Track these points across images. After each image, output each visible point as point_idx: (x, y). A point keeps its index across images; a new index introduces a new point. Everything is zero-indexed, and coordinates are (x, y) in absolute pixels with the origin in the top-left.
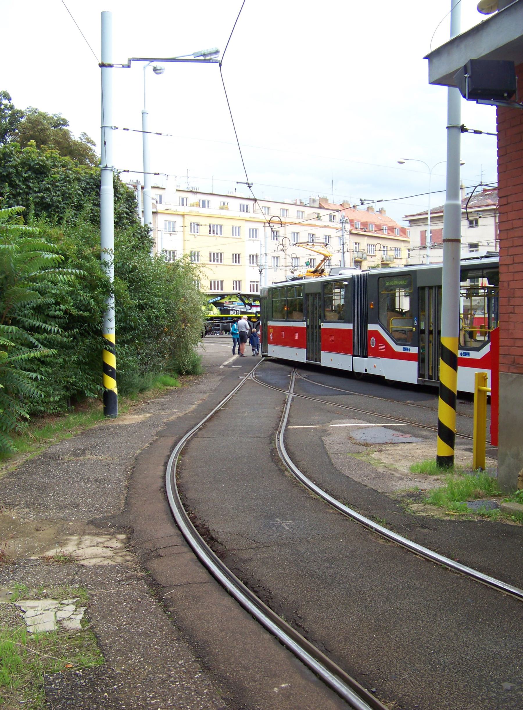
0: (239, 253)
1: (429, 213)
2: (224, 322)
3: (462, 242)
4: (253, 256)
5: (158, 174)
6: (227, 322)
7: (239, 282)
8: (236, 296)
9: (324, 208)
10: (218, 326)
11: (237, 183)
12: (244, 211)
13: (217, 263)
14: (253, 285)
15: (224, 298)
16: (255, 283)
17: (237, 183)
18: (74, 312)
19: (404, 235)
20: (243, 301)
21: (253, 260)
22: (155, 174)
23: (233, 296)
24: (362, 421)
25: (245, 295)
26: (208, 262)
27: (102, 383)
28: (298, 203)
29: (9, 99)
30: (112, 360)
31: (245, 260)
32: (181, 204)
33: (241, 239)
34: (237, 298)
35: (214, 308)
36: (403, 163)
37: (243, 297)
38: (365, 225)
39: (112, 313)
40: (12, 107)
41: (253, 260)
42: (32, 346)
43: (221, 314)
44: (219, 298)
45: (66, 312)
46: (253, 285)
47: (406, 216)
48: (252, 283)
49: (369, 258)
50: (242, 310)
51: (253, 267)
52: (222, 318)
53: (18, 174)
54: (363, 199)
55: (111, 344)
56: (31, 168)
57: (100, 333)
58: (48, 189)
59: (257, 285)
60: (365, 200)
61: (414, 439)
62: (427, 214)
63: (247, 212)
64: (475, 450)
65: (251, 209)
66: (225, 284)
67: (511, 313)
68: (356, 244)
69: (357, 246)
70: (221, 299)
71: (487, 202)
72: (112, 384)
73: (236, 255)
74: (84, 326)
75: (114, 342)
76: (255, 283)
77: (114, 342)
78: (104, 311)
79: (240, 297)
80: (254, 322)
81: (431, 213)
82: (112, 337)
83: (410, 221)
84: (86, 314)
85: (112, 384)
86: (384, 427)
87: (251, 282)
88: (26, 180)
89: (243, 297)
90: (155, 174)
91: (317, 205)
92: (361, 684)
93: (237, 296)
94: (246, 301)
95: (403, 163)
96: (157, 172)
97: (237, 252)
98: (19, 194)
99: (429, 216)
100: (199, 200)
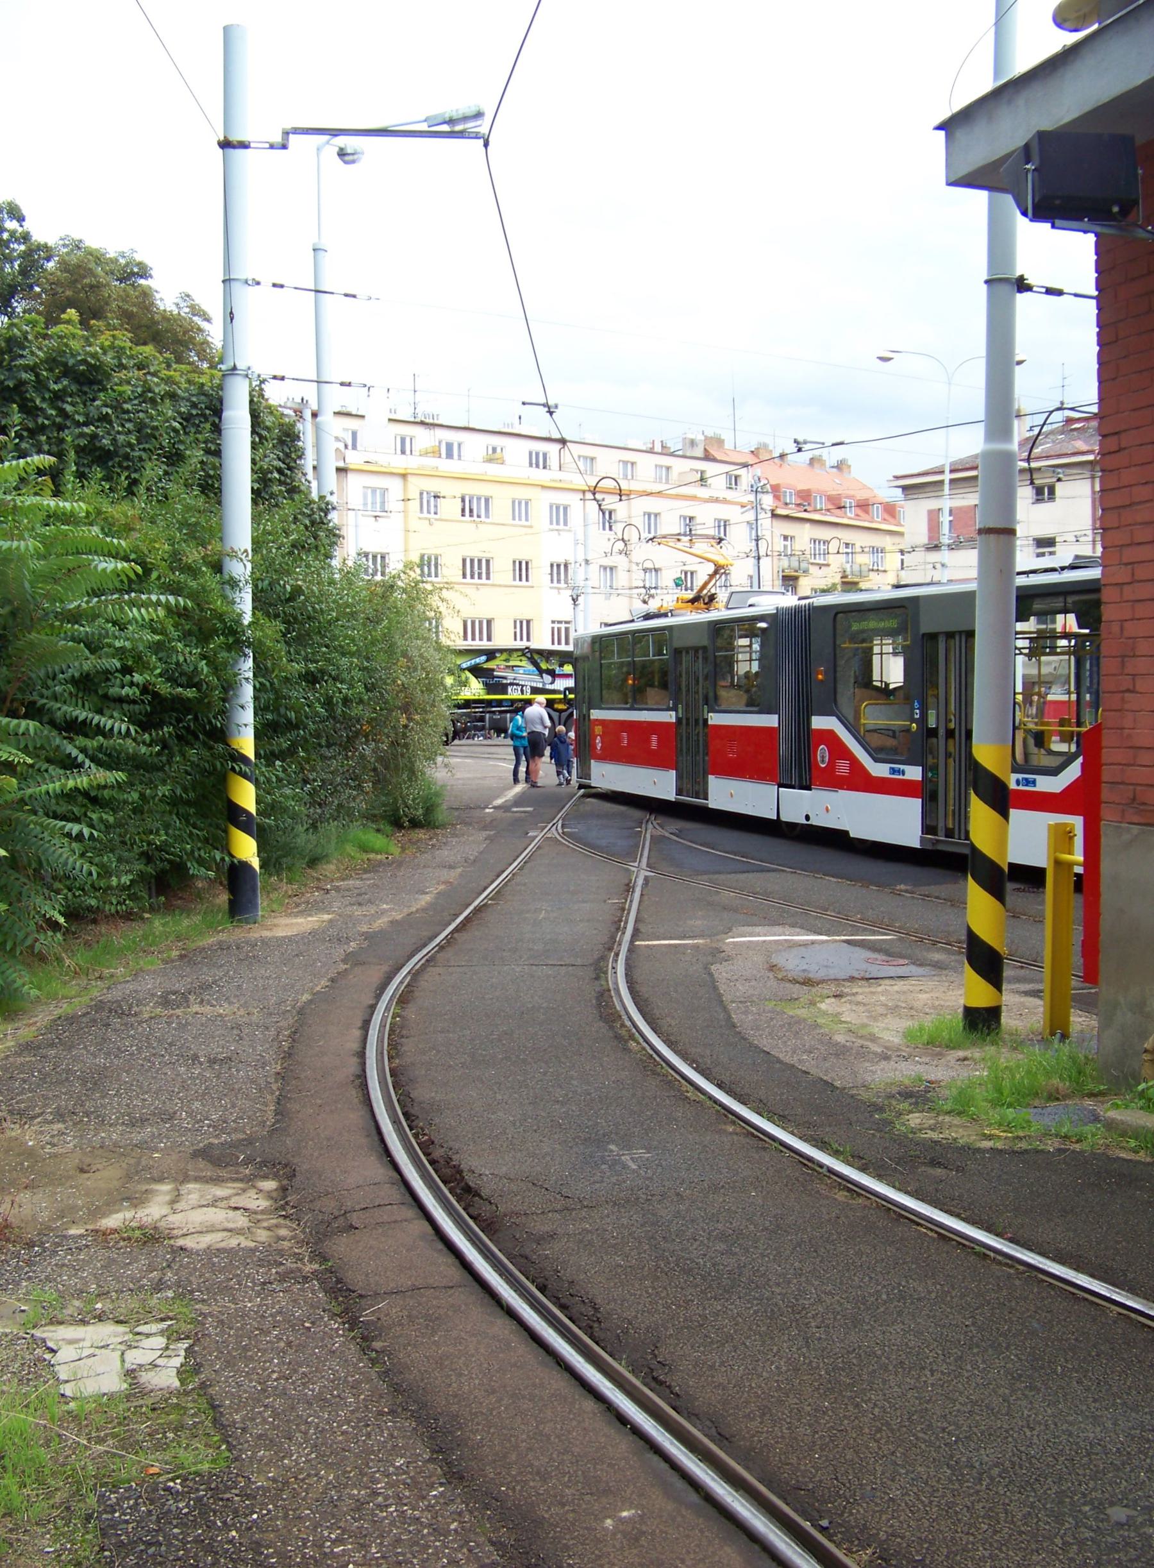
0: (527, 558)
1: (947, 470)
2: (494, 712)
3: (1019, 534)
4: (558, 566)
5: (349, 384)
6: (501, 712)
7: (528, 622)
8: (520, 653)
9: (715, 460)
10: (482, 719)
11: (524, 403)
12: (537, 466)
13: (480, 581)
14: (559, 629)
15: (494, 658)
16: (563, 626)
17: (524, 403)
18: (164, 688)
20: (535, 664)
21: (559, 573)
22: (342, 384)
23: (515, 654)
24: (798, 930)
25: (540, 652)
26: (460, 579)
27: (225, 846)
28: (658, 448)
29: (21, 219)
30: (246, 796)
31: (540, 573)
32: (399, 451)
33: (531, 527)
34: (523, 658)
35: (472, 679)
36: (889, 359)
37: (536, 657)
38: (805, 497)
39: (247, 692)
40: (26, 237)
41: (559, 573)
42: (70, 765)
43: (488, 694)
44: (484, 658)
45: (145, 689)
46: (559, 629)
47: (897, 478)
48: (556, 626)
49: (813, 570)
50: (534, 685)
51: (559, 589)
52: (489, 703)
53: (40, 385)
54: (800, 439)
55: (244, 759)
56: (68, 372)
57: (221, 735)
58: (105, 418)
59: (567, 630)
60: (805, 442)
61: (913, 969)
63: (545, 467)
64: (1047, 995)
65: (553, 461)
66: (495, 627)
67: (1128, 691)
68: (786, 538)
69: (789, 543)
70: (487, 661)
71: (1074, 447)
72: (246, 848)
73: (520, 563)
74: (185, 719)
75: (251, 755)
76: (563, 626)
77: (251, 755)
78: (229, 687)
79: (529, 655)
80: (560, 711)
82: (246, 743)
83: (905, 488)
84: (190, 693)
85: (246, 848)
86: (848, 942)
87: (553, 622)
88: (58, 397)
89: (536, 657)
90: (342, 384)
91: (699, 452)
92: (796, 1510)
93: (524, 655)
94: (544, 666)
95: (889, 359)
96: (347, 380)
97: (523, 557)
98: (42, 429)
100: (440, 442)
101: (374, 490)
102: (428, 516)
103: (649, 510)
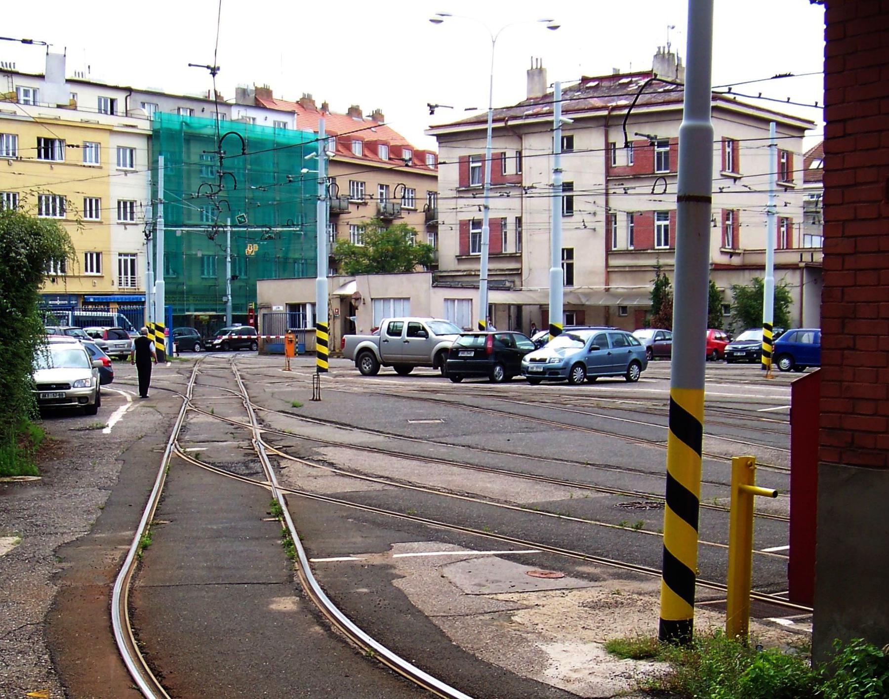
1: (490, 121)
3: (675, 198)
4: (125, 203)
5: (30, 42)
7: (98, 255)
9: (264, 108)
11: (190, 65)
12: (106, 113)
14: (126, 261)
16: (129, 258)
17: (190, 65)
19: (345, 152)
22: (24, 41)
24: (456, 546)
28: (212, 98)
31: (110, 213)
32: (109, 112)
33: (100, 168)
36: (441, 21)
46: (126, 261)
47: (432, 127)
48: (123, 258)
49: (352, 208)
51: (125, 224)
54: (433, 104)
59: (133, 261)
60: (437, 106)
61: (571, 582)
62: (486, 122)
63: (112, 113)
64: (730, 607)
65: (120, 107)
67: (848, 348)
68: (382, 187)
69: (383, 191)
71: (590, 103)
76: (129, 258)
81: (494, 121)
83: (439, 137)
86: (501, 556)
87: (120, 255)
90: (24, 41)
91: (251, 102)
95: (441, 21)
96: (29, 38)
99: (490, 126)
100: (17, 89)
101: (125, 149)
102: (125, 168)
103: (40, 136)
